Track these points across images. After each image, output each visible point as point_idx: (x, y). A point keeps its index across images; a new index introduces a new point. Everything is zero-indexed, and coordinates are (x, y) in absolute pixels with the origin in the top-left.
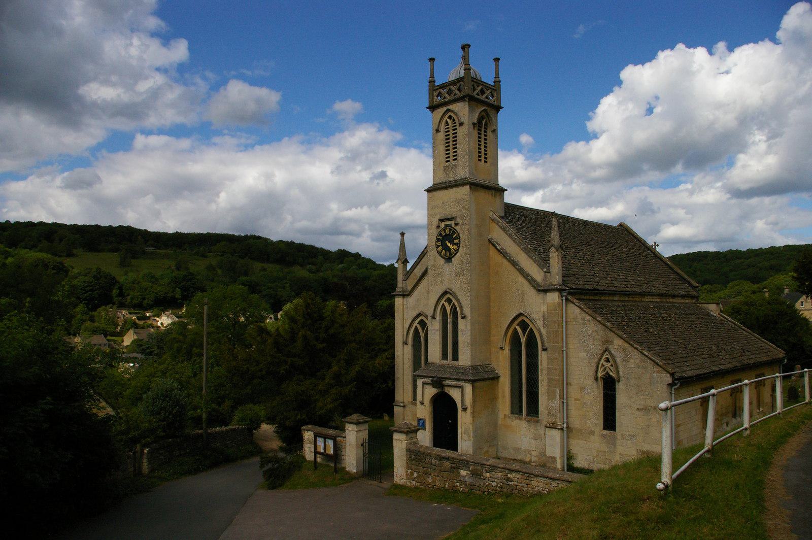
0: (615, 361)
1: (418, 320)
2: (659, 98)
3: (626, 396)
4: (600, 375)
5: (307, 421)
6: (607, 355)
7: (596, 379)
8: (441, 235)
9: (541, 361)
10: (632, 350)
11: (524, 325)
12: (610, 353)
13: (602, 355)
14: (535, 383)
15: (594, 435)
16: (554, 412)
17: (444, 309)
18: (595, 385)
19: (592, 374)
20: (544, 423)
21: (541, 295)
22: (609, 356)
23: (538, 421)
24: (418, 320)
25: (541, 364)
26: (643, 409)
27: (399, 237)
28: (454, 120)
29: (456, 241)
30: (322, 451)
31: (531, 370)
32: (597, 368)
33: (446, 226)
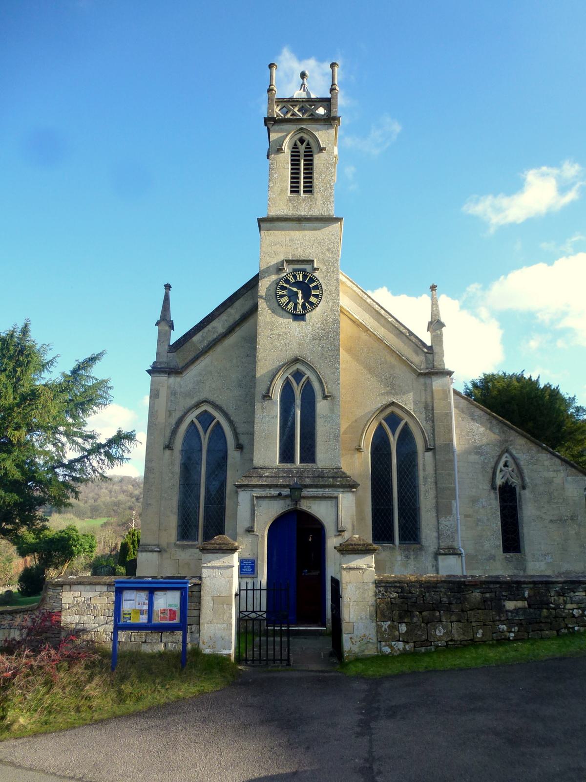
0: (517, 465)
1: (210, 410)
2: (170, 287)
3: (535, 506)
4: (499, 482)
5: (562, 594)
6: (506, 457)
7: (493, 487)
8: (316, 288)
9: (424, 465)
10: (177, 482)
11: (393, 420)
12: (511, 455)
13: (500, 457)
14: (413, 497)
15: (494, 560)
16: (449, 533)
17: (287, 390)
18: (492, 495)
19: (487, 486)
20: (236, 556)
21: (422, 380)
22: (510, 459)
23: (421, 549)
24: (198, 412)
25: (424, 470)
26: (557, 520)
27: (163, 291)
28: (308, 144)
29: (313, 299)
30: (144, 619)
31: (405, 479)
32: (494, 473)
33: (295, 270)
